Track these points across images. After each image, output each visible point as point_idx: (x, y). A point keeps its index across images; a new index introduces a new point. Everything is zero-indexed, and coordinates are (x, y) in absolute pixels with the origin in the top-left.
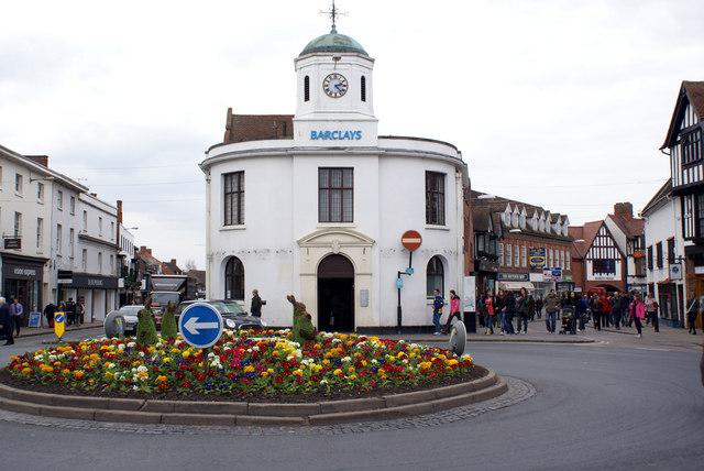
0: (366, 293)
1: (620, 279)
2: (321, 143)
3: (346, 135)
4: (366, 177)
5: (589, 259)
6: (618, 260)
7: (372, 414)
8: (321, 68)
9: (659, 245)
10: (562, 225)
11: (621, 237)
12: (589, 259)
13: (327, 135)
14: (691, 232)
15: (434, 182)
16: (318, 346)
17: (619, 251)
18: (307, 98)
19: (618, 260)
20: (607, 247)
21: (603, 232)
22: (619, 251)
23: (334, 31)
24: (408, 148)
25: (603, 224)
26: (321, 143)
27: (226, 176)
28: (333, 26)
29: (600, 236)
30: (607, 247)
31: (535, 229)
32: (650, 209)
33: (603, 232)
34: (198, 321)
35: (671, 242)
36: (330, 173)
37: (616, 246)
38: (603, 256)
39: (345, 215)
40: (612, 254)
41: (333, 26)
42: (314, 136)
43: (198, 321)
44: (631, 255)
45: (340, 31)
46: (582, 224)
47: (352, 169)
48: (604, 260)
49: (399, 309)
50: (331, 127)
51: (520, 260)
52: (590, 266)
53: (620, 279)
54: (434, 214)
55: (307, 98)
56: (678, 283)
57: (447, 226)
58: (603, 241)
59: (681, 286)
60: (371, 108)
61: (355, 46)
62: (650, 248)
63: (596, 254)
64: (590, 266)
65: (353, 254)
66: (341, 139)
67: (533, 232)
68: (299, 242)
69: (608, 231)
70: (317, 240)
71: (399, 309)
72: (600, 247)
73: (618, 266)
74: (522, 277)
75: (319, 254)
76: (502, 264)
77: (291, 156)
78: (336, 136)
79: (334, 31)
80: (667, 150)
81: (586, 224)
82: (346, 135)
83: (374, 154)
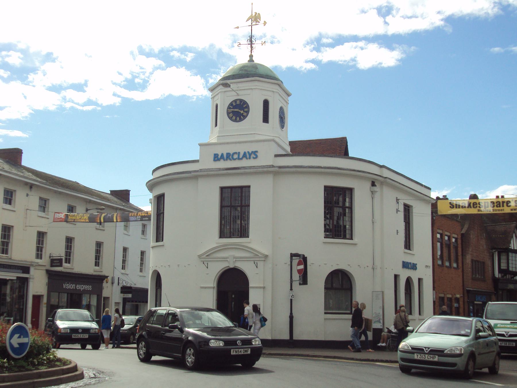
0: (36, 292)
2: (222, 164)
3: (245, 155)
6: (130, 216)
13: (229, 157)
16: (38, 358)
18: (216, 125)
19: (130, 216)
23: (251, 60)
26: (222, 164)
28: (251, 56)
34: (19, 337)
36: (231, 191)
41: (251, 56)
42: (216, 158)
43: (19, 337)
45: (257, 60)
49: (291, 317)
50: (231, 149)
55: (216, 125)
57: (356, 240)
65: (247, 268)
66: (239, 159)
70: (202, 257)
71: (291, 317)
77: (196, 178)
78: (236, 156)
79: (251, 60)
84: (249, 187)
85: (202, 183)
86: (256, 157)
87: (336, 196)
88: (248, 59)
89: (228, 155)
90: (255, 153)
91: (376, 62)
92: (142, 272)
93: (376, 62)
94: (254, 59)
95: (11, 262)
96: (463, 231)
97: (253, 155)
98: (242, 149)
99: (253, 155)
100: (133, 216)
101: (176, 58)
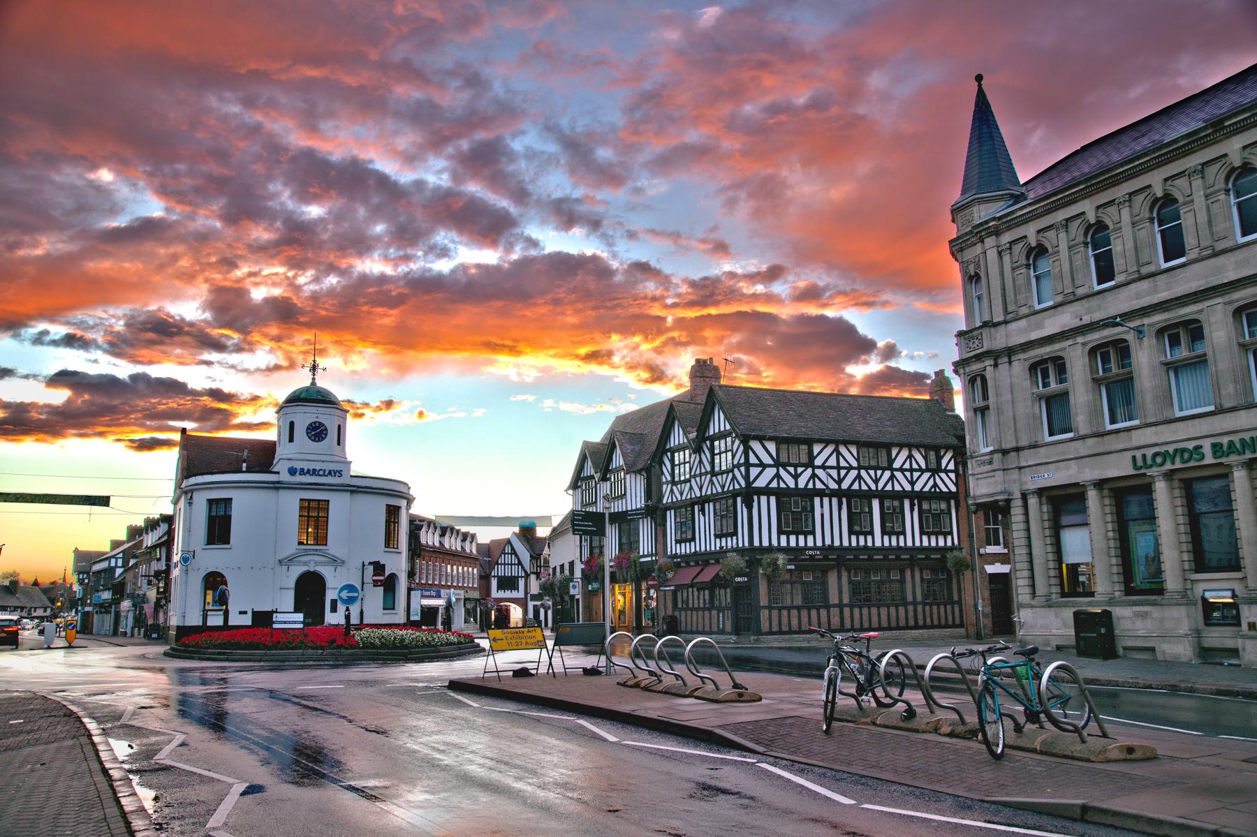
1: (523, 596)
2: (298, 478)
3: (330, 473)
4: (339, 505)
5: (494, 577)
6: (522, 577)
7: (419, 682)
8: (305, 416)
9: (562, 566)
10: (471, 542)
11: (525, 556)
12: (494, 577)
14: (586, 555)
15: (393, 512)
17: (523, 567)
19: (522, 577)
20: (511, 564)
21: (508, 549)
22: (523, 567)
23: (313, 383)
24: (374, 486)
25: (508, 542)
27: (210, 502)
29: (505, 554)
30: (511, 564)
31: (447, 546)
32: (557, 533)
33: (508, 549)
35: (572, 564)
37: (520, 563)
38: (508, 574)
39: (321, 539)
40: (516, 571)
44: (533, 573)
45: (320, 384)
46: (488, 542)
47: (328, 501)
48: (508, 577)
50: (318, 466)
51: (427, 577)
52: (494, 583)
53: (523, 596)
54: (390, 539)
55: (339, 426)
56: (577, 597)
58: (508, 558)
59: (578, 600)
60: (344, 450)
61: (333, 400)
62: (554, 569)
63: (500, 571)
64: (494, 583)
65: (326, 572)
66: (324, 475)
67: (466, 553)
68: (280, 562)
69: (513, 548)
72: (505, 564)
73: (521, 583)
74: (434, 594)
75: (297, 571)
76: (417, 581)
79: (313, 383)
80: (571, 492)
81: (492, 541)
82: (330, 473)
83: (347, 491)
84: (231, 499)
85: (284, 495)
86: (341, 475)
87: (820, 555)
88: (311, 381)
89: (314, 470)
90: (340, 472)
91: (579, 366)
92: (108, 498)
93: (579, 366)
94: (316, 381)
95: (86, 675)
96: (1041, 648)
97: (337, 474)
98: (328, 467)
99: (337, 474)
100: (793, 607)
101: (265, 336)
